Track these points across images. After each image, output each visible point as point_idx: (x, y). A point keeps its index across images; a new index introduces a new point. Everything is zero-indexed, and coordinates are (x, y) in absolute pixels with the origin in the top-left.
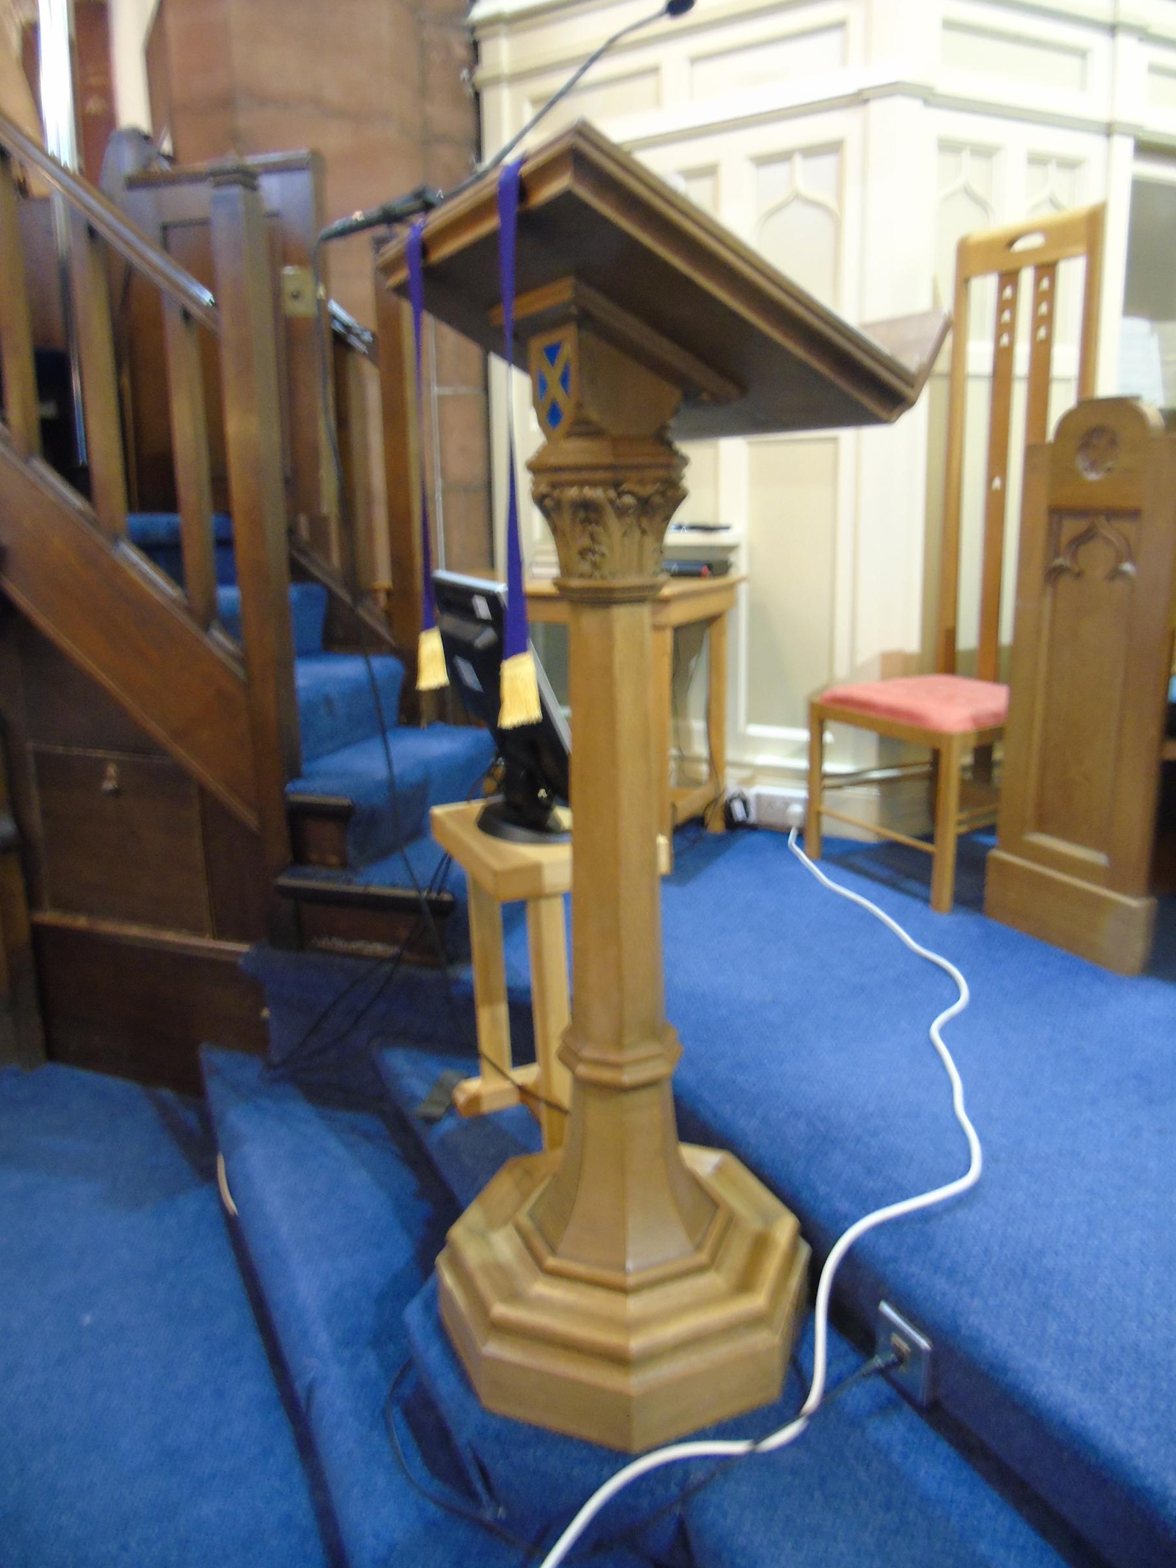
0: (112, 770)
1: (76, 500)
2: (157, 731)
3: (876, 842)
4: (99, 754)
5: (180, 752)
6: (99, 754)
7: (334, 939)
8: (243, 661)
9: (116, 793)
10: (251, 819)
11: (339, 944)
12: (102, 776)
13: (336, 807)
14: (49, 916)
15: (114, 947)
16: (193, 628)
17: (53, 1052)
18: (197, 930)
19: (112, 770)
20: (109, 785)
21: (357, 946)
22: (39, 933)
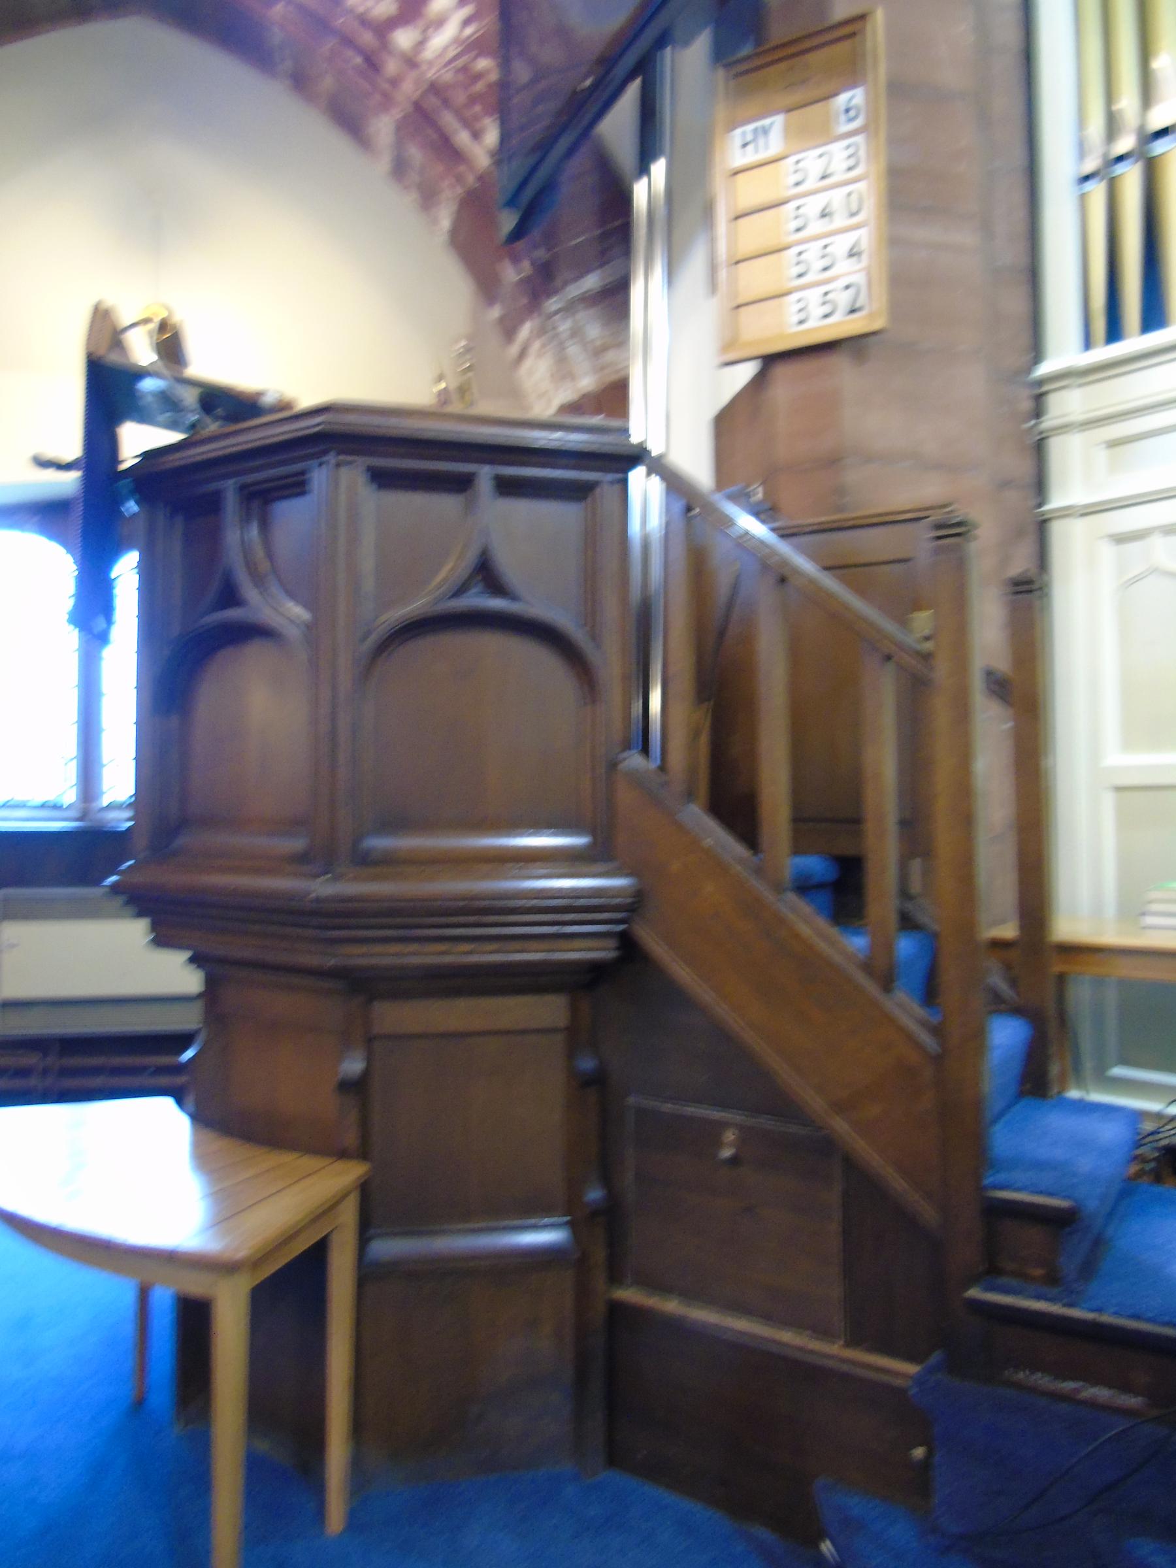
0: (730, 1136)
1: (739, 849)
2: (814, 1102)
3: (136, 387)
4: (716, 1114)
5: (840, 1126)
6: (716, 1114)
7: (1039, 1375)
8: (937, 1031)
9: (734, 1161)
10: (928, 1214)
11: (1042, 1380)
12: (718, 1144)
13: (520, 961)
14: (629, 1294)
15: (676, 1327)
16: (872, 988)
17: (614, 1458)
18: (823, 1332)
19: (730, 1136)
20: (727, 1153)
21: (1069, 1386)
22: (616, 1310)
